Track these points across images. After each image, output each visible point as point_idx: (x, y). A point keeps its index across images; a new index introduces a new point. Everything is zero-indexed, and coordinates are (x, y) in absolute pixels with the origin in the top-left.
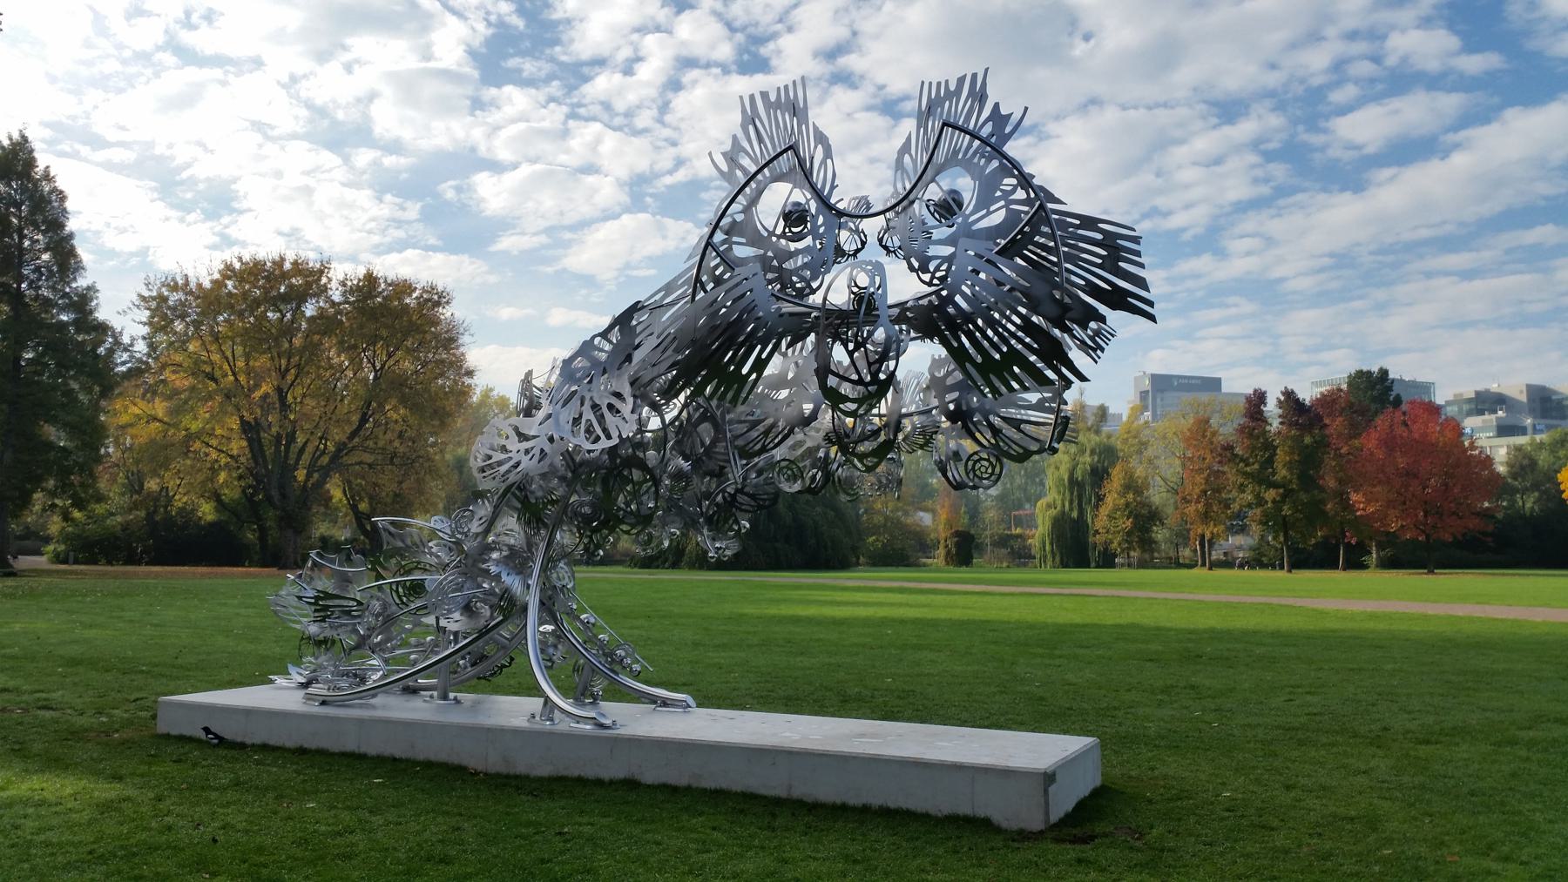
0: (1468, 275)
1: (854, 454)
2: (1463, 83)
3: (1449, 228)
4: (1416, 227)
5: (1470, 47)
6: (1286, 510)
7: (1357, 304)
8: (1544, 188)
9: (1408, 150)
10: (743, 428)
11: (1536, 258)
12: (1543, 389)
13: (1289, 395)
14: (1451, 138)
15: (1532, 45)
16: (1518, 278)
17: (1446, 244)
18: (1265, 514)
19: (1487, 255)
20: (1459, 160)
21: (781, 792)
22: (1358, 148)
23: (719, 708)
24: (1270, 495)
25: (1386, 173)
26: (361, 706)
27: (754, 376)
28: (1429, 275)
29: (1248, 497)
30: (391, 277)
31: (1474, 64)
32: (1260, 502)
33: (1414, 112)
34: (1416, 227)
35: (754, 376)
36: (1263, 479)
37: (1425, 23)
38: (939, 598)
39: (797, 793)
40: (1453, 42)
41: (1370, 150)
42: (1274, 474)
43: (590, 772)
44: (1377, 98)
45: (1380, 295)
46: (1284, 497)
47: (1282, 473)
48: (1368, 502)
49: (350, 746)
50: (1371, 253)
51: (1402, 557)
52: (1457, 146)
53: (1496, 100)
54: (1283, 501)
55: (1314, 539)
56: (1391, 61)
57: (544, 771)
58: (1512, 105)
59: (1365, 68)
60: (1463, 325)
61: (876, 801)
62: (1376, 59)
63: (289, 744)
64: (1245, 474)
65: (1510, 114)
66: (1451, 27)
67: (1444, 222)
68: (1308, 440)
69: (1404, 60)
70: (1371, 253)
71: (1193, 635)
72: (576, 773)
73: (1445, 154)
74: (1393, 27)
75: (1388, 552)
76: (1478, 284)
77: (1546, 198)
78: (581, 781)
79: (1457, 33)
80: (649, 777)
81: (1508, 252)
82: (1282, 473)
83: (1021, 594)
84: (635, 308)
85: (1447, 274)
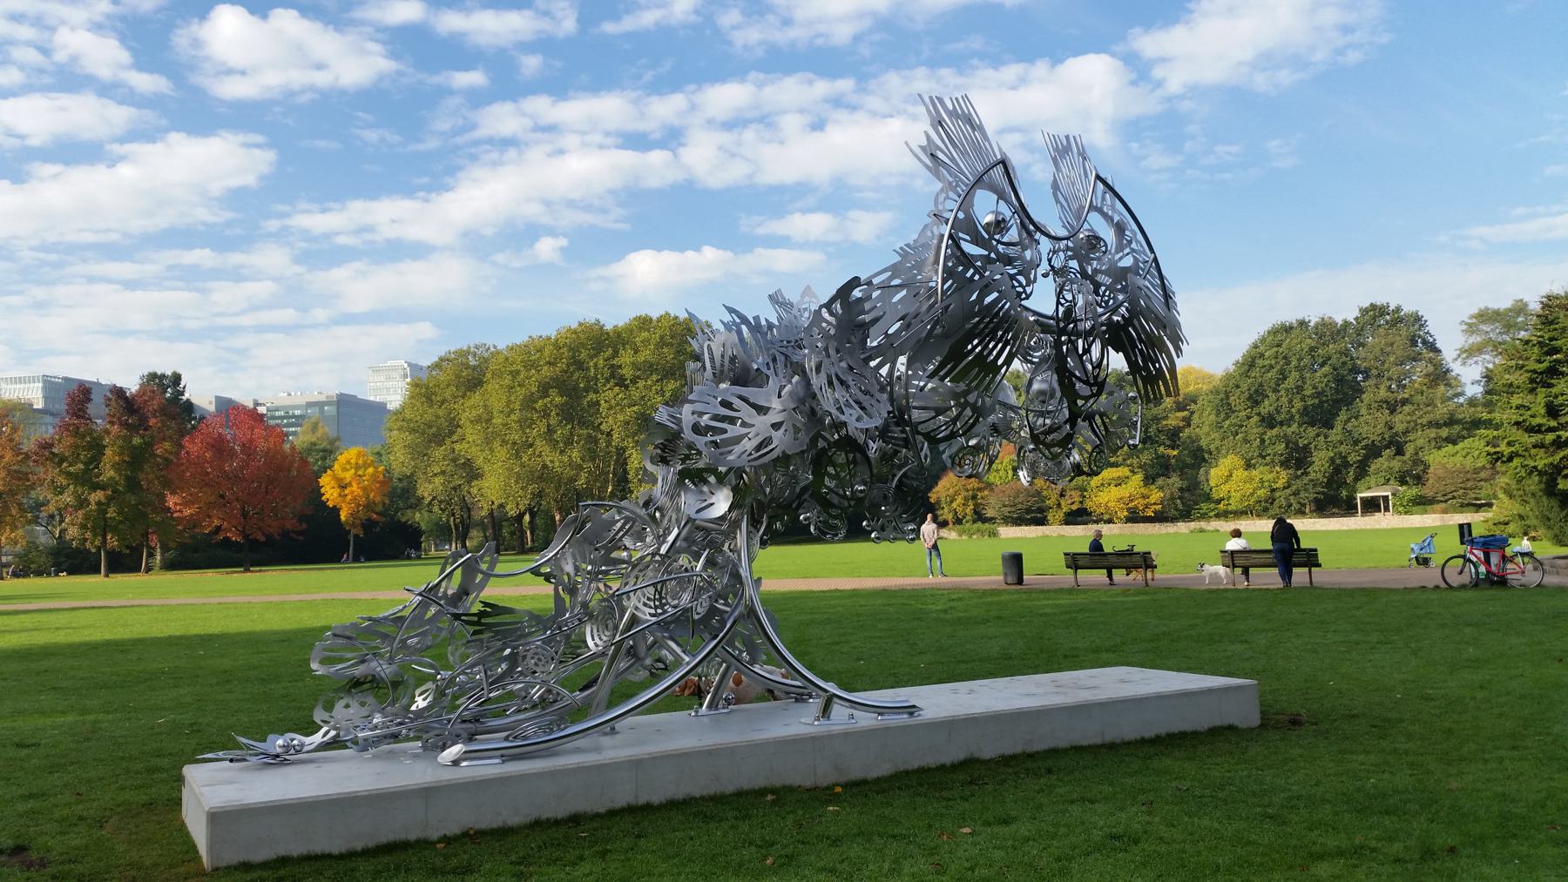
0: (131, 285)
1: (1043, 443)
2: (128, 97)
3: (114, 237)
4: (81, 230)
5: (139, 66)
7: (14, 300)
8: (203, 214)
9: (74, 152)
10: (926, 415)
11: (193, 277)
12: (229, 401)
14: (117, 149)
15: (196, 80)
16: (178, 294)
17: (110, 252)
18: (87, 517)
19: (150, 269)
20: (124, 170)
21: (1098, 740)
22: (21, 137)
23: (1082, 668)
24: (97, 496)
25: (51, 169)
26: (578, 750)
28: (92, 279)
29: (67, 498)
31: (144, 82)
33: (83, 114)
34: (81, 230)
36: (87, 480)
37: (97, 27)
38: (52, 617)
39: (1108, 738)
40: (124, 56)
41: (34, 142)
43: (931, 761)
44: (44, 89)
45: (40, 293)
46: (110, 499)
47: (108, 473)
49: (622, 797)
50: (32, 249)
52: (122, 158)
53: (164, 122)
56: (60, 57)
57: (884, 769)
58: (178, 130)
59: (31, 56)
60: (126, 333)
61: (1162, 730)
62: (45, 51)
63: (602, 810)
64: (69, 474)
65: (175, 137)
66: (123, 39)
67: (109, 230)
68: (137, 441)
69: (74, 59)
70: (32, 249)
71: (285, 632)
72: (916, 764)
73: (113, 162)
74: (63, 22)
75: (171, 554)
76: (139, 295)
77: (205, 224)
78: (1183, 735)
79: (129, 49)
80: (988, 751)
81: (171, 268)
82: (108, 473)
84: (854, 282)
85: (110, 281)
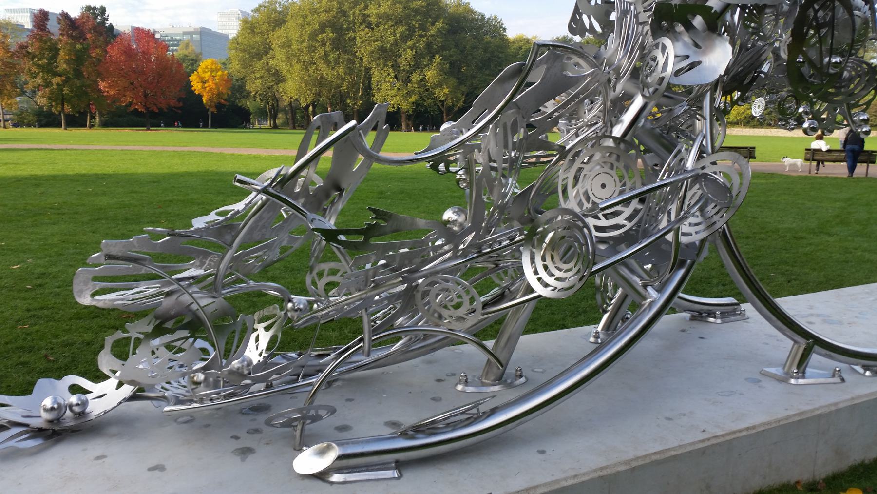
6: (66, 91)
13: (65, 16)
18: (52, 92)
24: (57, 80)
27: (342, 237)
29: (39, 81)
30: (823, 476)
32: (48, 84)
35: (342, 237)
36: (49, 70)
42: (57, 67)
46: (65, 82)
47: (63, 66)
48: (110, 87)
51: (120, 118)
54: (64, 86)
55: (73, 109)
68: (78, 46)
82: (63, 66)
83: (493, 412)
